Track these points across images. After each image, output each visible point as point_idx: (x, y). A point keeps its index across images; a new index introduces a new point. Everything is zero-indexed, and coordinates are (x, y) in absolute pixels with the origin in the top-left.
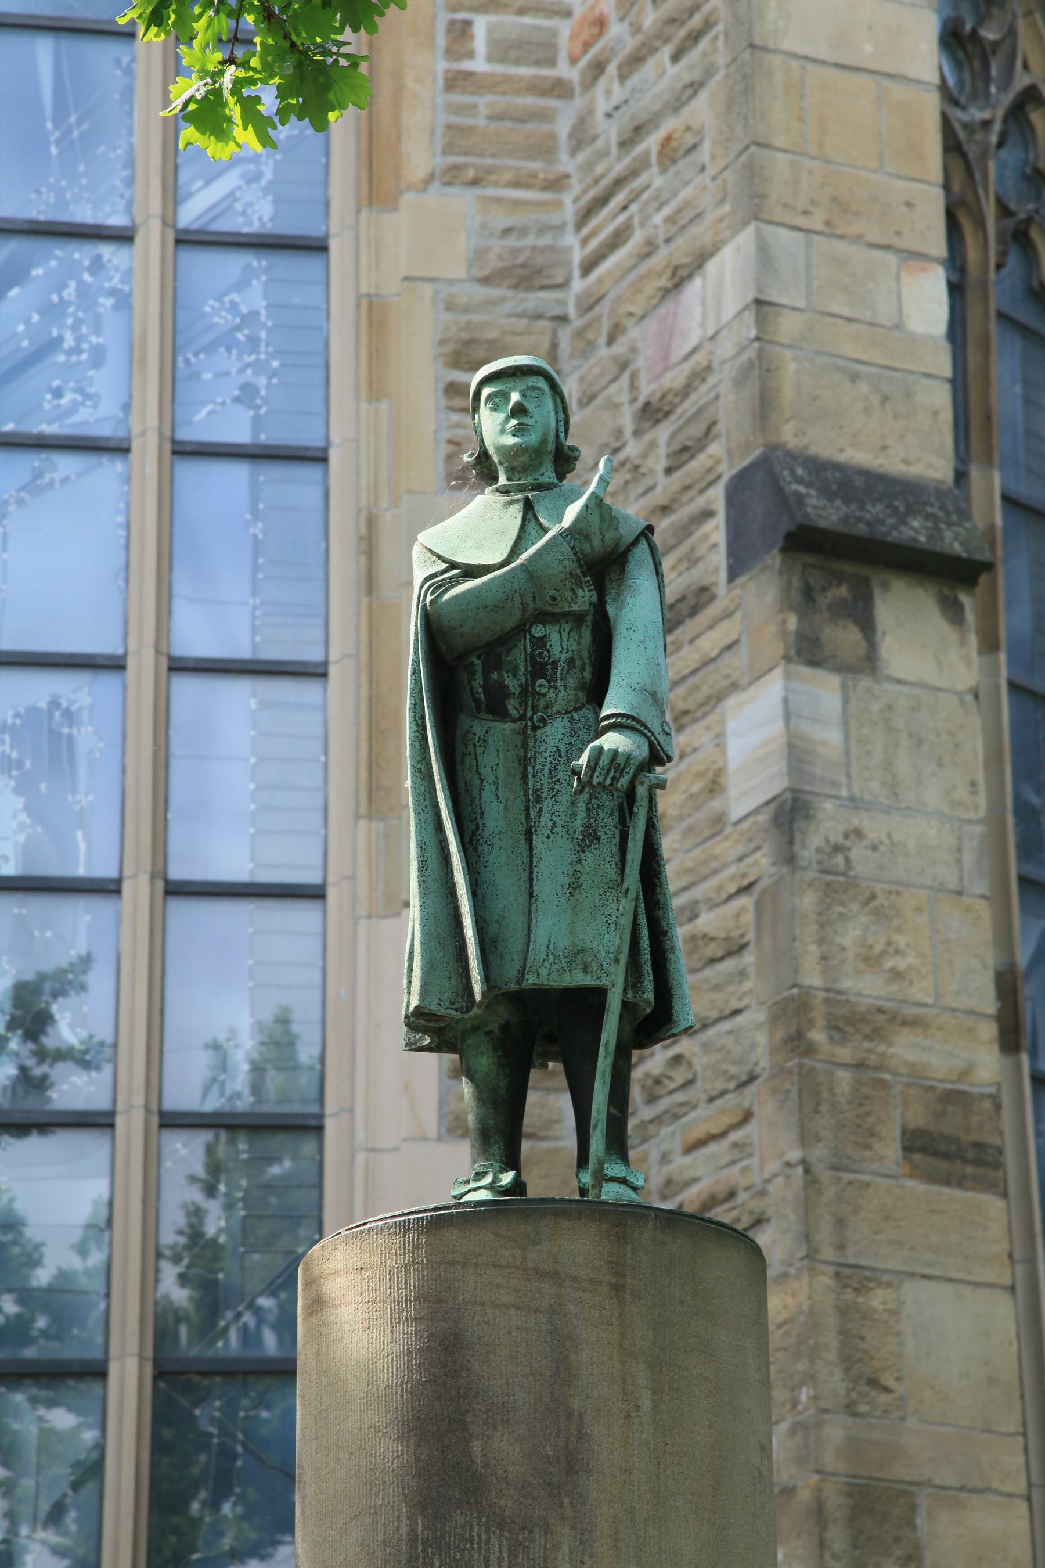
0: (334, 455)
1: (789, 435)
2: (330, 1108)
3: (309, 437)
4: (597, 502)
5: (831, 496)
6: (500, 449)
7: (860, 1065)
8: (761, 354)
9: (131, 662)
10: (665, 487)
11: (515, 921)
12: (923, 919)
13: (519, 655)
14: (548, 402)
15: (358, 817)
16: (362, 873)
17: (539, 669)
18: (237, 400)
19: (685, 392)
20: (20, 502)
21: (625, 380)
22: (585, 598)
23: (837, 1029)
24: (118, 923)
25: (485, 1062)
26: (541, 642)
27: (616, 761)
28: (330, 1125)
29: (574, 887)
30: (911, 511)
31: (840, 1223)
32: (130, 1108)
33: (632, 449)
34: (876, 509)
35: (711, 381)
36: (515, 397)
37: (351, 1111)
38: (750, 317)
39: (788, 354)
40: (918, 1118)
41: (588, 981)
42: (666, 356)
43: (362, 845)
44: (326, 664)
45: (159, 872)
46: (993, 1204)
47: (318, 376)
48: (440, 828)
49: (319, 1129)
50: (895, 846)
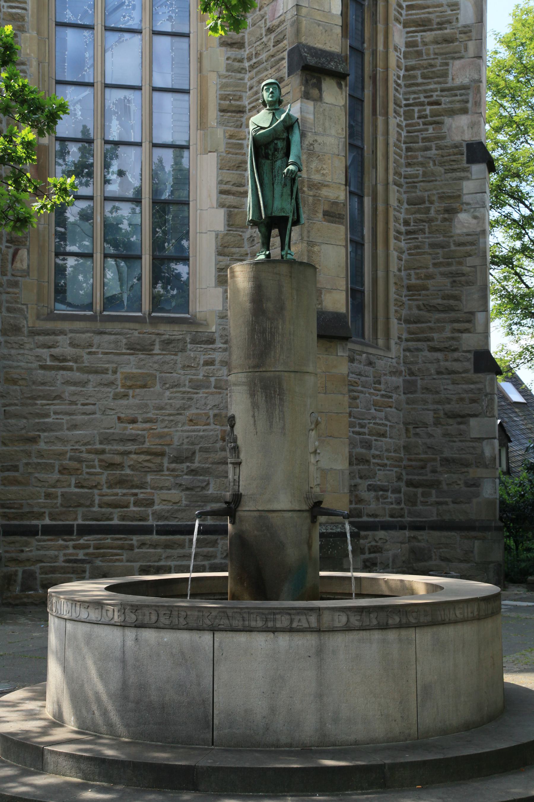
0: (191, 35)
1: (303, 40)
2: (191, 199)
3: (185, 30)
4: (288, 114)
5: (313, 56)
6: (268, 101)
7: (314, 196)
8: (297, 18)
9: (143, 88)
10: (273, 50)
11: (270, 202)
12: (330, 161)
13: (272, 147)
14: (278, 90)
15: (197, 129)
16: (199, 143)
17: (276, 150)
18: (167, 20)
19: (278, 26)
20: (116, 45)
21: (263, 21)
22: (285, 135)
23: (310, 187)
24: (142, 153)
25: (263, 229)
26: (276, 144)
27: (292, 172)
28: (191, 204)
29: (282, 195)
30: (331, 60)
31: (309, 232)
32: (145, 198)
33: (265, 39)
34: (323, 60)
35: (285, 24)
36: (271, 90)
37: (196, 200)
38: (295, 8)
39: (304, 19)
40: (327, 208)
41: (284, 215)
42: (274, 16)
43: (198, 137)
44: (189, 90)
45: (151, 141)
46: (342, 228)
47: (188, 14)
48: (256, 182)
49: (189, 204)
50: (324, 144)
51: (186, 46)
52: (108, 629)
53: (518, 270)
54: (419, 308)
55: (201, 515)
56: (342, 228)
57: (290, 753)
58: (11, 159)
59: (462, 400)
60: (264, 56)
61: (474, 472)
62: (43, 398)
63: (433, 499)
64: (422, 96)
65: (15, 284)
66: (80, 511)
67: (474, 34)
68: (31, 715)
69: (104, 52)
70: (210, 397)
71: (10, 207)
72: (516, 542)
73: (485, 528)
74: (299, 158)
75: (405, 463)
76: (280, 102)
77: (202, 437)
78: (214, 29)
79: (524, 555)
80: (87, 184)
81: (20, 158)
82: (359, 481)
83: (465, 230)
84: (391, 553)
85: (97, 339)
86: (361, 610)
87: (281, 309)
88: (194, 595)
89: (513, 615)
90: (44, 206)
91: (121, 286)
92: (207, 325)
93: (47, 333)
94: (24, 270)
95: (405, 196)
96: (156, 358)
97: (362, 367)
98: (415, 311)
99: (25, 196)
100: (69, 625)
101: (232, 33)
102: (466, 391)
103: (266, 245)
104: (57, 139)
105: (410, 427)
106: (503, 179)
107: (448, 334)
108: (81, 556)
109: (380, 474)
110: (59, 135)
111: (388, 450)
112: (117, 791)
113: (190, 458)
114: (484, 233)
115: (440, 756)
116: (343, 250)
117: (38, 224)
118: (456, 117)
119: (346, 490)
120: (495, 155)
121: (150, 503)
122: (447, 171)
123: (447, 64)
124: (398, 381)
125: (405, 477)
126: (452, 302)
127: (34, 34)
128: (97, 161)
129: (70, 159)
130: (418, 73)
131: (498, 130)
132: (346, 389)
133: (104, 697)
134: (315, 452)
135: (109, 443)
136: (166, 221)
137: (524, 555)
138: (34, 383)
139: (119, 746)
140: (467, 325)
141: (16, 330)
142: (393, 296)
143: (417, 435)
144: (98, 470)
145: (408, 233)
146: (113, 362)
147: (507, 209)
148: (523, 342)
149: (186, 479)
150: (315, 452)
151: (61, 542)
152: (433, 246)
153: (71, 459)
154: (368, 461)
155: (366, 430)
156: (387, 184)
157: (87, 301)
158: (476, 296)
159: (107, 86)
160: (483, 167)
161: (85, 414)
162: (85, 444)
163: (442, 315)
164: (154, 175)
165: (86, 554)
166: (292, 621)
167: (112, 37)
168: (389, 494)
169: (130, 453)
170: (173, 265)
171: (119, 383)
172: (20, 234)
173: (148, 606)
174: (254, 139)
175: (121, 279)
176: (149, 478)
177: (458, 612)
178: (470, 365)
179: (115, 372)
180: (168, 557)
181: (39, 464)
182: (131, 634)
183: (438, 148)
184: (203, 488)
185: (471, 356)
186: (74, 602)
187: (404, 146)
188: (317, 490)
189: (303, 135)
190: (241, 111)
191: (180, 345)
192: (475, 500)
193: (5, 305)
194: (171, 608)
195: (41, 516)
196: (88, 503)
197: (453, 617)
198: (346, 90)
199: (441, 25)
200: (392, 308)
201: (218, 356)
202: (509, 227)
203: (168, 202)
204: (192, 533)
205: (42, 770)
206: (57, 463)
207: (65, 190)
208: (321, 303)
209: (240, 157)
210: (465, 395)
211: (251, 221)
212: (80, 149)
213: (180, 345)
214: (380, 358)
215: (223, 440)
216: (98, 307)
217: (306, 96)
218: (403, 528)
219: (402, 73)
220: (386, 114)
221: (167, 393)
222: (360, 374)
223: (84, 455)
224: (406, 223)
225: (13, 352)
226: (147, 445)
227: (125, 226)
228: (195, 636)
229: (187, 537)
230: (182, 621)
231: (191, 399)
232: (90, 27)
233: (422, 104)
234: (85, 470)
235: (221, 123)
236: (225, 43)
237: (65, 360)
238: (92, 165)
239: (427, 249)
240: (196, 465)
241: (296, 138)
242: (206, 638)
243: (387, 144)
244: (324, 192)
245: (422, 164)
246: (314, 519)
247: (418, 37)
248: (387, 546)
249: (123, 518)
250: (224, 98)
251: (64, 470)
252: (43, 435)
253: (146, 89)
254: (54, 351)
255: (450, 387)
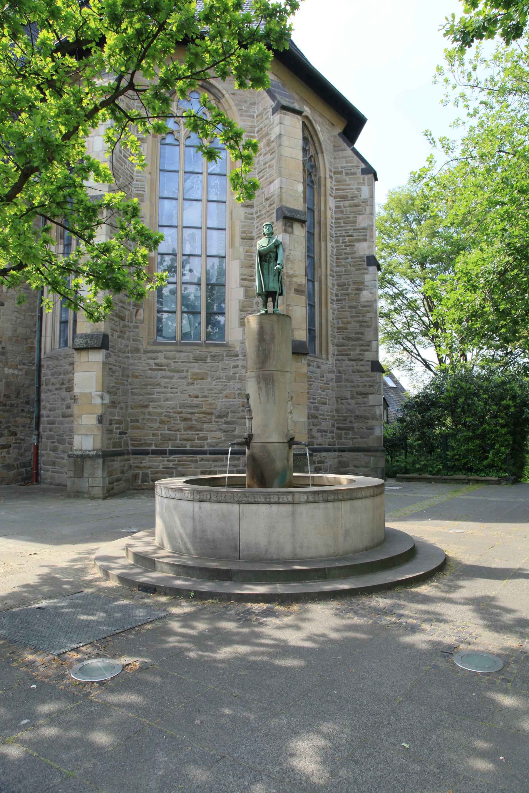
1: (284, 204)
3: (224, 200)
4: (277, 240)
10: (268, 209)
13: (268, 256)
17: (270, 257)
22: (275, 250)
23: (287, 277)
25: (264, 298)
27: (279, 269)
40: (296, 287)
45: (206, 254)
46: (304, 297)
51: (224, 207)
52: (185, 503)
53: (393, 320)
54: (343, 339)
55: (233, 445)
56: (304, 297)
57: (278, 563)
58: (136, 264)
59: (365, 385)
60: (263, 212)
61: (371, 422)
62: (151, 385)
63: (350, 436)
64: (344, 232)
65: (137, 327)
66: (170, 443)
67: (369, 203)
68: (148, 544)
69: (183, 210)
70: (236, 385)
71: (135, 288)
72: (391, 457)
73: (376, 451)
74: (282, 261)
75: (336, 418)
76: (272, 234)
77: (232, 405)
78: (239, 199)
79: (395, 464)
80: (173, 276)
81: (140, 263)
82: (312, 427)
83: (366, 299)
84: (328, 464)
85: (178, 355)
86: (314, 493)
87: (273, 339)
88: (229, 486)
89: (390, 493)
90: (152, 287)
91: (190, 327)
92: (235, 347)
93: (153, 352)
94: (141, 320)
95: (336, 282)
96: (208, 364)
97: (314, 369)
98: (341, 340)
99: (142, 282)
100: (166, 500)
101: (248, 201)
102: (367, 381)
103: (265, 305)
104: (159, 254)
105: (339, 399)
106: (384, 275)
107: (358, 352)
108: (171, 466)
109: (324, 424)
110: (160, 252)
111: (327, 411)
112: (192, 581)
113: (226, 416)
114: (375, 301)
115: (354, 563)
116: (305, 309)
117: (149, 296)
118: (361, 243)
119: (306, 432)
120: (380, 262)
121: (206, 439)
122: (357, 270)
123: (356, 217)
124: (333, 376)
125: (336, 425)
126: (360, 336)
127: (149, 203)
128: (179, 265)
129: (165, 264)
130: (342, 221)
131: (382, 250)
132: (306, 380)
133: (184, 536)
134: (291, 412)
135: (184, 408)
136: (213, 294)
137: (395, 464)
138: (146, 377)
139: (193, 559)
140: (368, 348)
141: (137, 350)
142: (330, 332)
143: (342, 403)
144: (179, 422)
145: (337, 300)
146: (186, 366)
147: (387, 290)
148: (395, 357)
149: (224, 427)
150: (291, 412)
151: (161, 458)
152: (350, 307)
153: (165, 416)
154: (317, 417)
155: (316, 401)
156: (327, 275)
157: (173, 335)
158: (372, 333)
159: (184, 227)
160: (375, 268)
161: (172, 393)
162: (172, 409)
163: (355, 343)
164: (208, 273)
165: (174, 465)
166: (279, 499)
167: (187, 203)
168: (328, 434)
169: (195, 413)
170: (216, 317)
171: (189, 377)
172: (139, 302)
173: (205, 491)
174: (259, 252)
175: (190, 324)
176: (205, 426)
177: (363, 493)
178: (369, 368)
179: (187, 372)
180: (215, 466)
181: (149, 419)
182: (197, 504)
183: (352, 258)
184: (233, 431)
185: (369, 363)
186: (168, 489)
187: (335, 257)
188: (292, 432)
189: (284, 251)
190: (252, 239)
191: (221, 358)
192: (371, 437)
193: (132, 338)
194: (217, 492)
195: (150, 445)
196: (174, 438)
197: (360, 495)
198: (306, 229)
199: (353, 198)
200: (330, 339)
201: (240, 363)
202: (388, 298)
203: (213, 285)
204: (228, 454)
205: (154, 570)
206: (158, 419)
207: (163, 279)
208: (293, 336)
209: (251, 262)
210: (366, 383)
211: (258, 294)
212: (171, 260)
213: (221, 358)
214: (323, 364)
215: (243, 406)
216: (179, 338)
217: (285, 231)
218: (335, 451)
219: (333, 221)
220: (326, 241)
221: (214, 382)
222: (313, 373)
223: (172, 414)
224: (337, 295)
225: (136, 361)
226: (204, 409)
227: (192, 297)
228: (230, 506)
229: (225, 456)
230: (223, 498)
231: (226, 385)
232: (176, 199)
233: (344, 236)
234: (173, 422)
235: (242, 245)
236: (244, 206)
237: (162, 366)
238: (176, 267)
239: (347, 309)
240: (229, 419)
241: (280, 251)
242: (236, 506)
243: (326, 256)
244: (295, 279)
245: (344, 266)
246: (290, 447)
247: (341, 204)
248: (327, 460)
249: (192, 446)
250: (243, 232)
251: (161, 422)
252: (151, 404)
253: (204, 228)
254: (156, 361)
255: (359, 379)
